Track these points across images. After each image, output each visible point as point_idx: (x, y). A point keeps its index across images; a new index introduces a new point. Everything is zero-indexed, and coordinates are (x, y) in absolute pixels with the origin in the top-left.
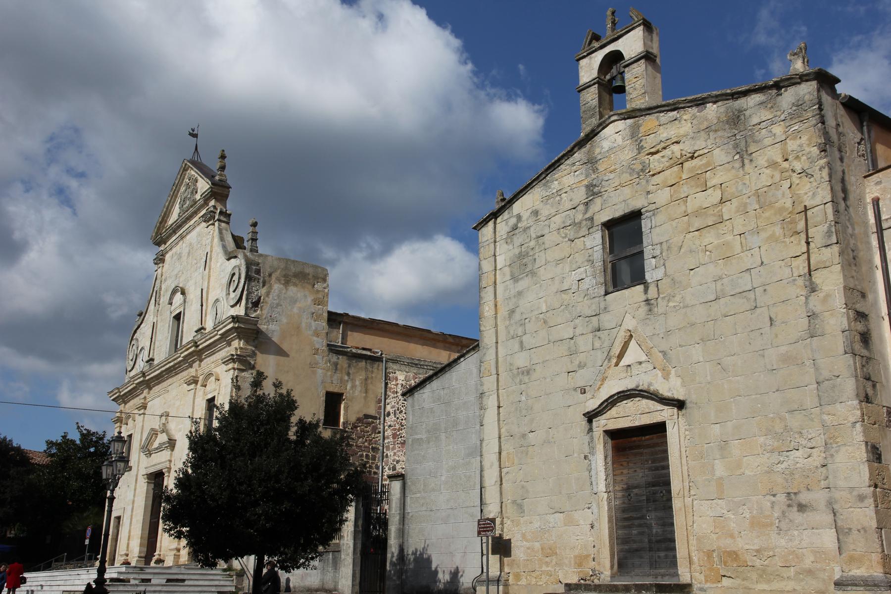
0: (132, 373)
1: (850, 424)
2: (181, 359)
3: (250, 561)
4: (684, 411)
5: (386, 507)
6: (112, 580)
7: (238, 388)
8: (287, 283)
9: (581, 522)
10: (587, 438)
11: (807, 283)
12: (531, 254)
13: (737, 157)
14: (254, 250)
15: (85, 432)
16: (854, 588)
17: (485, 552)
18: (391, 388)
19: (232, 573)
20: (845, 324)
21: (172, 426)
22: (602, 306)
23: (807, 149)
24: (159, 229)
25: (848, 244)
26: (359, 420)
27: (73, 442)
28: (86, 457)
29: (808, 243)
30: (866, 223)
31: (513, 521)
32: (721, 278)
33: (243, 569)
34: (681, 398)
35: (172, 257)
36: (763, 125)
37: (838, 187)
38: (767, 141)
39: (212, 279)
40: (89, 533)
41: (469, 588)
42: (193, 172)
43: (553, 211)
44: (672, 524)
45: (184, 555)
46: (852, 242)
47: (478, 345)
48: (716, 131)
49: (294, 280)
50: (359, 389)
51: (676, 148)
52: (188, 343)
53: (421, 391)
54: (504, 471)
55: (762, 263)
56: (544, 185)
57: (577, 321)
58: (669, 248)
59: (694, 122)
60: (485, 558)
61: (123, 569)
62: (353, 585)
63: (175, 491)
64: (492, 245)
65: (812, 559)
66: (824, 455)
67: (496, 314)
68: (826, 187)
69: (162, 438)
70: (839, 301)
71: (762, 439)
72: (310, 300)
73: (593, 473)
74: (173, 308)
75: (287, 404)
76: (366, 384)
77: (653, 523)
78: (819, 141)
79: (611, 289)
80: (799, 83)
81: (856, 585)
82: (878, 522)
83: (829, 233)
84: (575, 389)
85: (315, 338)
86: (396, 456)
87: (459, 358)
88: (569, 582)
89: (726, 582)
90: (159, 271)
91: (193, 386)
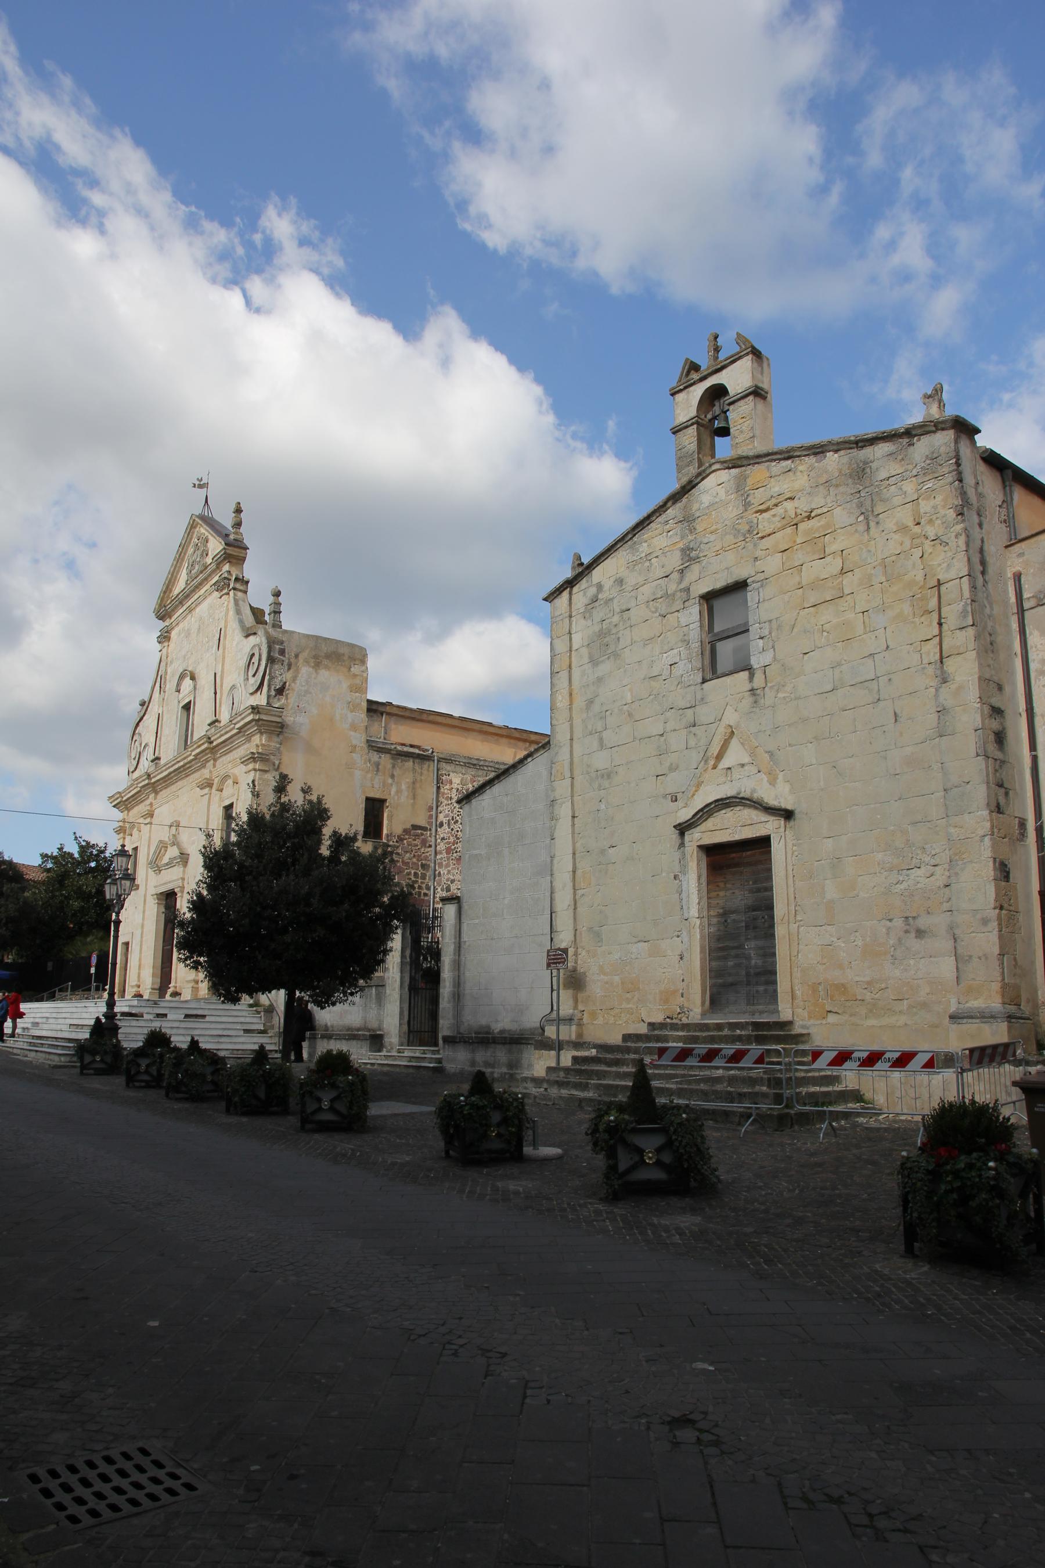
0: (136, 774)
1: (978, 838)
2: (192, 757)
3: (278, 997)
4: (792, 823)
5: (439, 935)
6: (123, 1014)
7: (256, 795)
8: (317, 665)
9: (669, 952)
10: (677, 855)
11: (939, 672)
12: (614, 631)
13: (861, 518)
14: (277, 625)
15: (84, 844)
16: (970, 1020)
17: (555, 987)
18: (444, 793)
19: (259, 1009)
20: (978, 721)
21: (184, 837)
22: (699, 697)
23: (942, 512)
24: (162, 599)
25: (985, 628)
26: (406, 831)
27: (71, 855)
28: (86, 873)
29: (940, 624)
30: (1006, 602)
31: (588, 952)
32: (839, 664)
33: (271, 1005)
34: (789, 807)
35: (179, 634)
36: (892, 480)
37: (976, 559)
38: (897, 500)
39: (227, 660)
40: (94, 960)
41: (536, 1029)
42: (203, 530)
43: (641, 580)
44: (774, 954)
45: (204, 988)
46: (990, 624)
47: (549, 742)
48: (837, 486)
49: (326, 662)
50: (405, 793)
51: (788, 505)
52: (200, 739)
53: (480, 798)
54: (579, 892)
55: (888, 647)
56: (631, 547)
57: (668, 714)
58: (779, 627)
59: (811, 474)
60: (555, 993)
61: (135, 1003)
62: (400, 1024)
63: (188, 915)
64: (567, 620)
65: (928, 990)
66: (947, 873)
67: (571, 704)
68: (962, 556)
69: (173, 852)
70: (973, 693)
71: (879, 856)
72: (345, 685)
73: (684, 895)
74: (181, 696)
75: (317, 814)
76: (414, 788)
77: (752, 953)
78: (956, 503)
79: (709, 676)
80: (934, 432)
81: (972, 1017)
82: (1001, 947)
83: (964, 614)
84: (665, 796)
85: (352, 733)
86: (448, 877)
87: (526, 757)
88: (653, 1020)
89: (832, 1019)
90: (164, 651)
91: (207, 790)
